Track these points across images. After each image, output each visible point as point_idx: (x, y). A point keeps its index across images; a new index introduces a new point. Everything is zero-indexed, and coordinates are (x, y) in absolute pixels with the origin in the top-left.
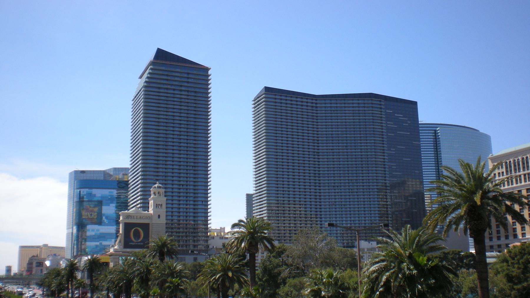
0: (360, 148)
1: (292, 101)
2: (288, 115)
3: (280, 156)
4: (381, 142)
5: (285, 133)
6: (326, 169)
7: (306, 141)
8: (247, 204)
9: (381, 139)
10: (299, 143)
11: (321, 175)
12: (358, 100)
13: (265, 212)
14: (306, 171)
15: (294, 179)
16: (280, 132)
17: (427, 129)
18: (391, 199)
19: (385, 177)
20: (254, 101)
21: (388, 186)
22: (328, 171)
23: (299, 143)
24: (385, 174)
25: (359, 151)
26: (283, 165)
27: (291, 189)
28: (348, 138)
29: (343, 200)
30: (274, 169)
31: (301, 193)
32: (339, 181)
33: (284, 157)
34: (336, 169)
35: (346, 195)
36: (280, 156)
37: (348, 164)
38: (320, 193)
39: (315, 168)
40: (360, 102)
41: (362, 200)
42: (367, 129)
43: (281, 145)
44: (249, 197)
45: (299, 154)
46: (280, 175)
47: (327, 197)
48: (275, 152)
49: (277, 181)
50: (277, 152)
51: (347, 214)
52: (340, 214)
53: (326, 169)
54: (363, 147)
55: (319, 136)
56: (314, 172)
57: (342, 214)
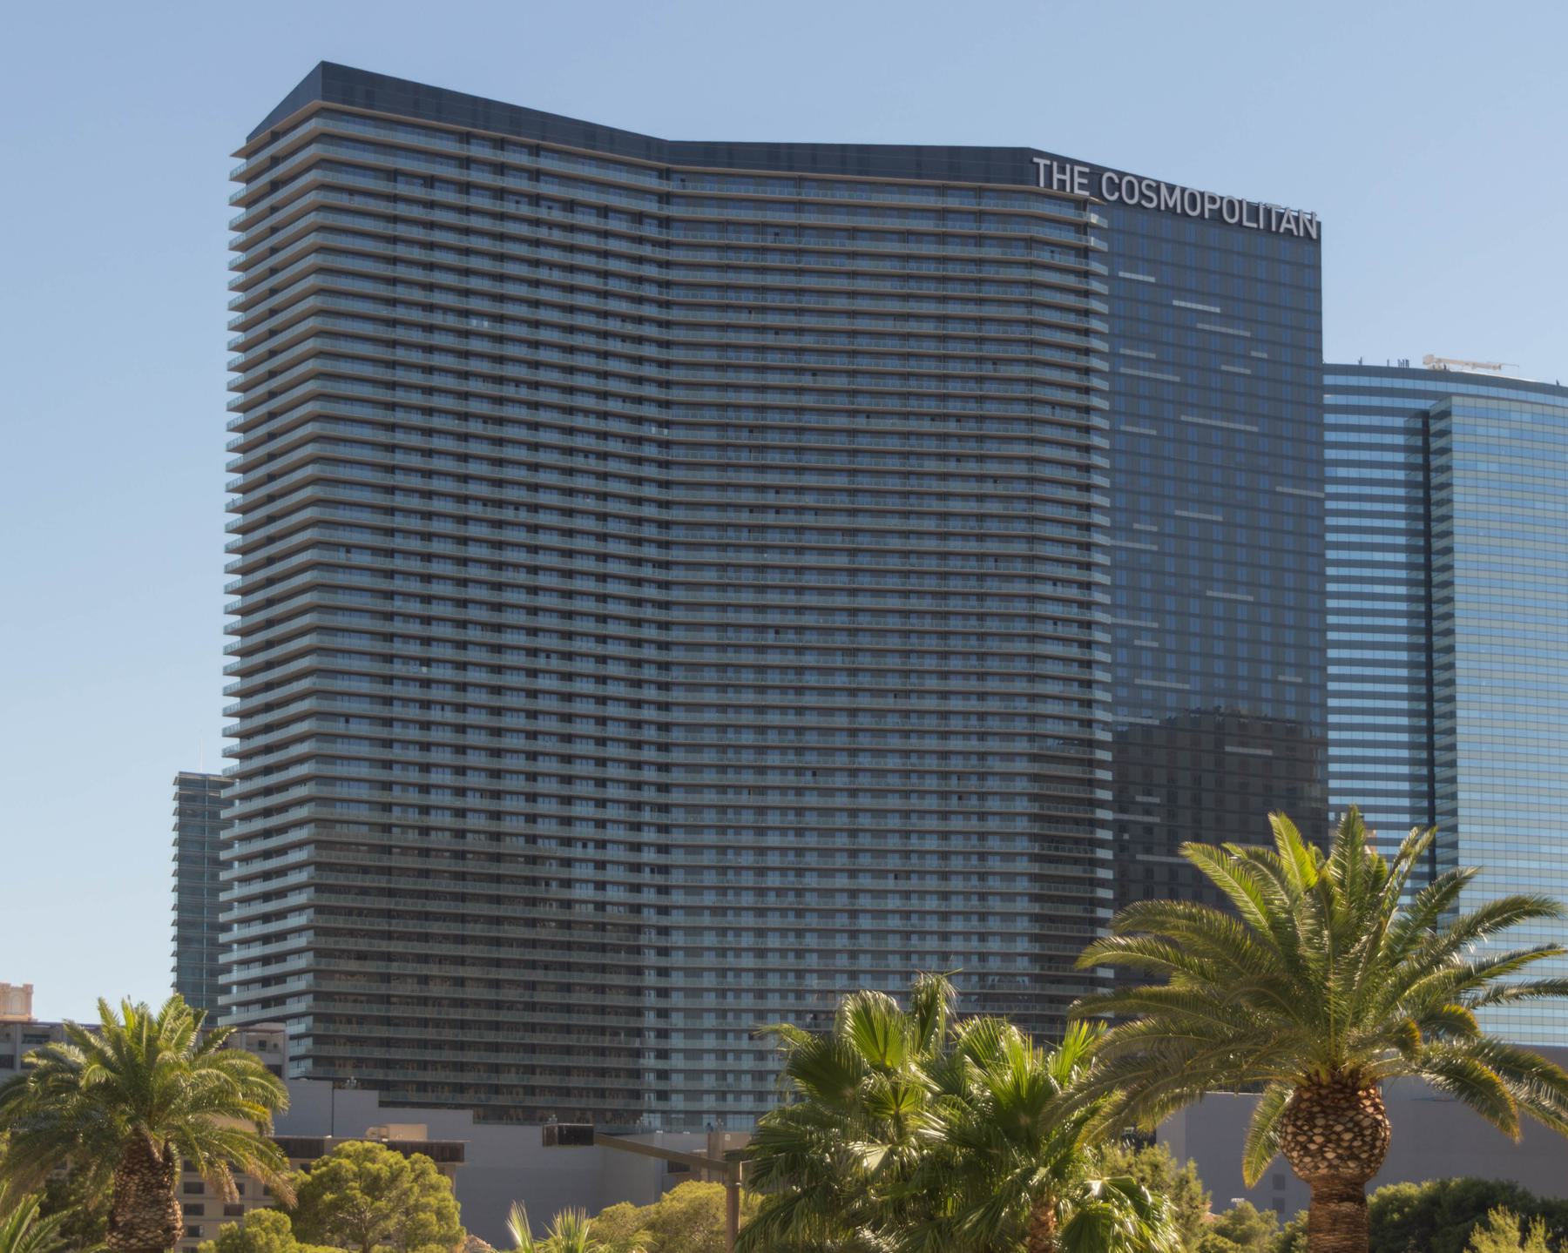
0: (936, 506)
1: (501, 169)
2: (475, 283)
3: (408, 596)
4: (1073, 475)
5: (450, 382)
6: (711, 636)
7: (590, 504)
8: (180, 939)
9: (1073, 456)
10: (543, 457)
11: (677, 736)
12: (942, 191)
13: (301, 877)
14: (579, 564)
15: (498, 607)
16: (415, 586)
17: (1375, 401)
18: (1120, 846)
19: (1088, 664)
20: (246, 153)
22: (723, 648)
23: (543, 457)
24: (1088, 645)
25: (930, 525)
26: (427, 620)
27: (473, 759)
28: (864, 621)
29: (811, 840)
30: (365, 623)
31: (541, 663)
32: (791, 719)
33: (437, 589)
34: (773, 678)
35: (829, 711)
36: (408, 533)
37: (853, 612)
38: (664, 706)
39: (638, 623)
40: (952, 202)
41: (932, 844)
42: (992, 606)
43: (415, 607)
44: (196, 797)
45: (534, 549)
46: (406, 701)
47: (710, 817)
48: (375, 529)
49: (388, 722)
50: (391, 490)
51: (830, 913)
52: (783, 932)
53: (711, 636)
54: (956, 506)
55: (674, 295)
56: (633, 796)
57: (800, 933)
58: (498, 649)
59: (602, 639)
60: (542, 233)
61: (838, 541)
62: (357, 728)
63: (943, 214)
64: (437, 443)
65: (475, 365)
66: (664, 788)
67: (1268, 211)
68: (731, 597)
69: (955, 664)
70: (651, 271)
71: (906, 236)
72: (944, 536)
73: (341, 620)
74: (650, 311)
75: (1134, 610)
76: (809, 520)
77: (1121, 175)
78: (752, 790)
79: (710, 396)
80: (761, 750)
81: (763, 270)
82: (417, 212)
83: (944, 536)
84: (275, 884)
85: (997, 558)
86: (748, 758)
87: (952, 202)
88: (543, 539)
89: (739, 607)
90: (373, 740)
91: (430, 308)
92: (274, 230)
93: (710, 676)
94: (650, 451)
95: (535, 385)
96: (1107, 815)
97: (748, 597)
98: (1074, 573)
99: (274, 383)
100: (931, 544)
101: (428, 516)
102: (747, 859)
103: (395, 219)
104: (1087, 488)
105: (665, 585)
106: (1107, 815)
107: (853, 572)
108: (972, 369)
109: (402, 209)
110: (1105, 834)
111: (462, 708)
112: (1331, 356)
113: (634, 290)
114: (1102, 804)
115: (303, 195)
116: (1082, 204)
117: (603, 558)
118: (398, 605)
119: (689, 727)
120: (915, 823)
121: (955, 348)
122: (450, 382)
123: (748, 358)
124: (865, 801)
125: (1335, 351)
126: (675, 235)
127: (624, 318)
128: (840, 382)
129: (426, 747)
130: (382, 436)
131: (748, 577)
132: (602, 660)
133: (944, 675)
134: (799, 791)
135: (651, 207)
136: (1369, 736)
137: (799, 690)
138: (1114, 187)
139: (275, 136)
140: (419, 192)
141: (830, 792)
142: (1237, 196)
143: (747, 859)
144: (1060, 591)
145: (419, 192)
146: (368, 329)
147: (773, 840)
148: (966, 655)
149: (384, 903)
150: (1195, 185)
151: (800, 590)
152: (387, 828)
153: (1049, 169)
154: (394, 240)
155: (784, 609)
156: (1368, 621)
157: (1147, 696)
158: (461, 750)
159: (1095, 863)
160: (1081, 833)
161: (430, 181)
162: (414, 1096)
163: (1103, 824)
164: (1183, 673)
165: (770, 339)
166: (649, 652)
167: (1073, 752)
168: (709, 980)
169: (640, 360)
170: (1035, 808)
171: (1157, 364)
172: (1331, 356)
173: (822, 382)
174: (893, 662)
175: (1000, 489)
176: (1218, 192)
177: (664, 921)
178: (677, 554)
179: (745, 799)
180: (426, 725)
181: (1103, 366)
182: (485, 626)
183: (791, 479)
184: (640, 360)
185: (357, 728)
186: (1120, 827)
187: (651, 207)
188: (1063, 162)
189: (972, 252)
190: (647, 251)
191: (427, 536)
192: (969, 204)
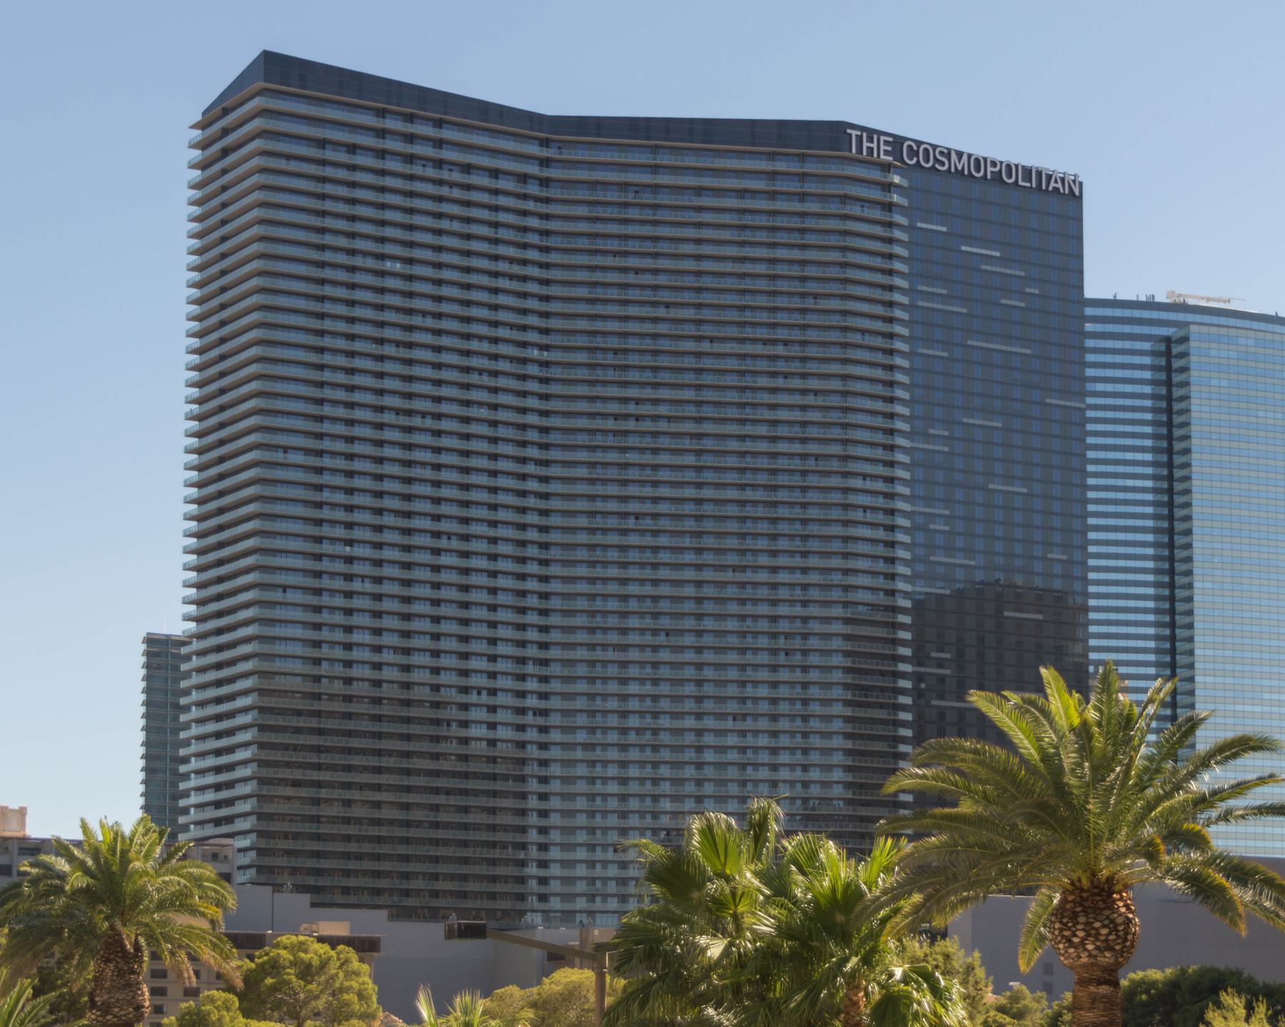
0: (767, 414)
1: (410, 138)
2: (389, 232)
3: (334, 488)
4: (879, 389)
5: (369, 313)
6: (582, 521)
7: (484, 413)
8: (148, 770)
9: (879, 374)
10: (445, 375)
11: (555, 603)
12: (772, 156)
13: (246, 719)
14: (474, 462)
15: (408, 498)
16: (340, 481)
17: (1127, 329)
18: (918, 694)
19: (892, 544)
20: (202, 126)
21: (903, 611)
22: (592, 531)
23: (445, 375)
24: (891, 528)
25: (762, 430)
26: (350, 508)
27: (388, 622)
28: (708, 509)
29: (665, 689)
30: (299, 510)
31: (443, 543)
32: (648, 590)
33: (358, 482)
34: (634, 556)
35: (679, 583)
36: (334, 437)
37: (699, 502)
38: (544, 579)
39: (523, 510)
40: (781, 166)
41: (763, 691)
42: (813, 497)
43: (340, 498)
44: (161, 653)
45: (438, 450)
46: (333, 575)
47: (582, 670)
48: (307, 434)
49: (318, 592)
50: (320, 402)
51: (680, 749)
52: (642, 764)
53: (582, 521)
54: (783, 415)
55: (552, 242)
56: (519, 652)
57: (655, 765)
58: (408, 532)
59: (494, 524)
60: (445, 191)
61: (687, 443)
62: (292, 596)
63: (773, 175)
64: (358, 363)
65: (389, 299)
66: (544, 646)
67: (1039, 173)
68: (599, 489)
69: (783, 544)
70: (533, 222)
71: (742, 193)
72: (773, 439)
73: (279, 508)
74: (532, 255)
75: (929, 500)
76: (663, 426)
77: (919, 143)
78: (616, 647)
79: (582, 324)
80: (624, 615)
81: (625, 221)
82: (342, 174)
83: (773, 439)
84: (225, 725)
85: (817, 457)
86: (613, 621)
87: (781, 166)
88: (445, 442)
89: (606, 498)
90: (305, 607)
91: (352, 252)
92: (224, 189)
93: (582, 554)
94: (533, 370)
95: (439, 316)
96: (907, 668)
97: (613, 490)
98: (880, 470)
99: (225, 314)
100: (763, 446)
101: (351, 423)
102: (613, 704)
103: (324, 180)
104: (891, 400)
105: (545, 480)
106: (907, 668)
107: (699, 469)
108: (796, 303)
109: (329, 172)
110: (906, 684)
111: (378, 580)
112: (1091, 291)
113: (520, 238)
114: (903, 659)
115: (248, 160)
116: (886, 168)
117: (494, 457)
118: (326, 496)
119: (565, 596)
120: (750, 674)
121: (783, 286)
122: (369, 313)
123: (613, 293)
124: (709, 657)
125: (1094, 287)
126: (553, 193)
127: (512, 260)
128: (689, 313)
129: (349, 612)
130: (313, 358)
131: (613, 473)
132: (493, 541)
133: (774, 553)
134: (655, 649)
135: (533, 169)
136: (1122, 603)
137: (655, 566)
138: (913, 153)
139: (226, 112)
140: (343, 157)
141: (680, 649)
142: (1014, 161)
143: (613, 704)
144: (869, 485)
145: (343, 157)
146: (301, 270)
147: (633, 688)
148: (792, 537)
149: (314, 740)
150: (979, 152)
151: (656, 484)
152: (317, 679)
153: (860, 138)
154: (323, 197)
155: (642, 499)
156: (1121, 509)
157: (940, 570)
158: (378, 614)
159: (898, 707)
160: (886, 683)
161: (352, 149)
162: (339, 899)
163: (904, 675)
164: (969, 552)
165: (631, 278)
166: (532, 535)
167: (879, 617)
168: (581, 804)
169: (524, 295)
170: (848, 663)
171: (948, 298)
172: (1091, 291)
173: (673, 313)
174: (732, 543)
175: (820, 401)
176: (999, 158)
177: (544, 755)
178: (555, 454)
179: (610, 655)
180: (349, 595)
181: (904, 300)
182: (397, 513)
183: (648, 393)
184: (524, 295)
185: (292, 596)
186: (918, 678)
187: (533, 169)
188: (871, 133)
189: (796, 206)
190: (530, 205)
191: (350, 440)
192: (794, 167)
